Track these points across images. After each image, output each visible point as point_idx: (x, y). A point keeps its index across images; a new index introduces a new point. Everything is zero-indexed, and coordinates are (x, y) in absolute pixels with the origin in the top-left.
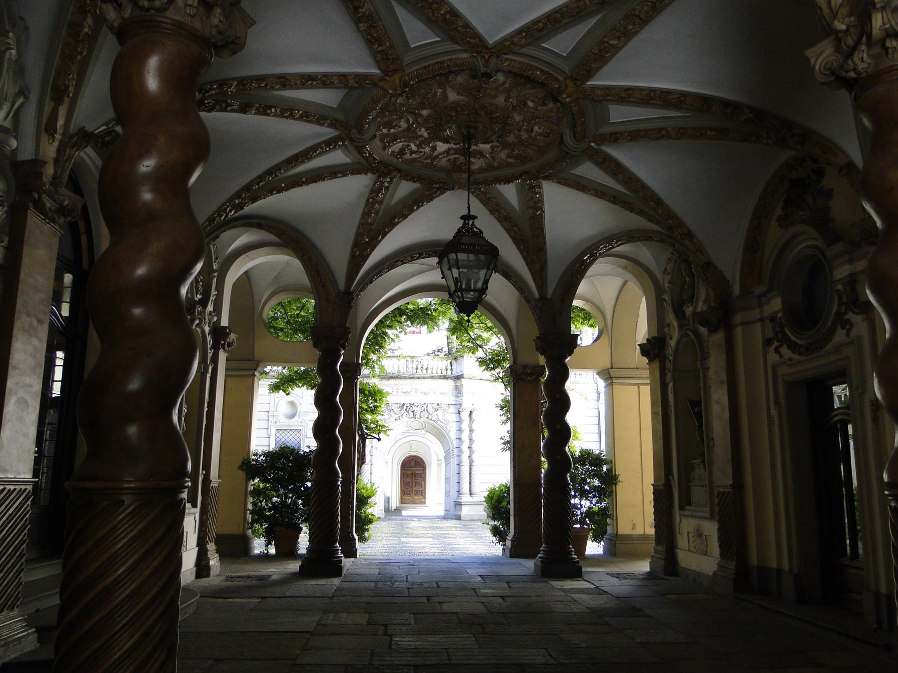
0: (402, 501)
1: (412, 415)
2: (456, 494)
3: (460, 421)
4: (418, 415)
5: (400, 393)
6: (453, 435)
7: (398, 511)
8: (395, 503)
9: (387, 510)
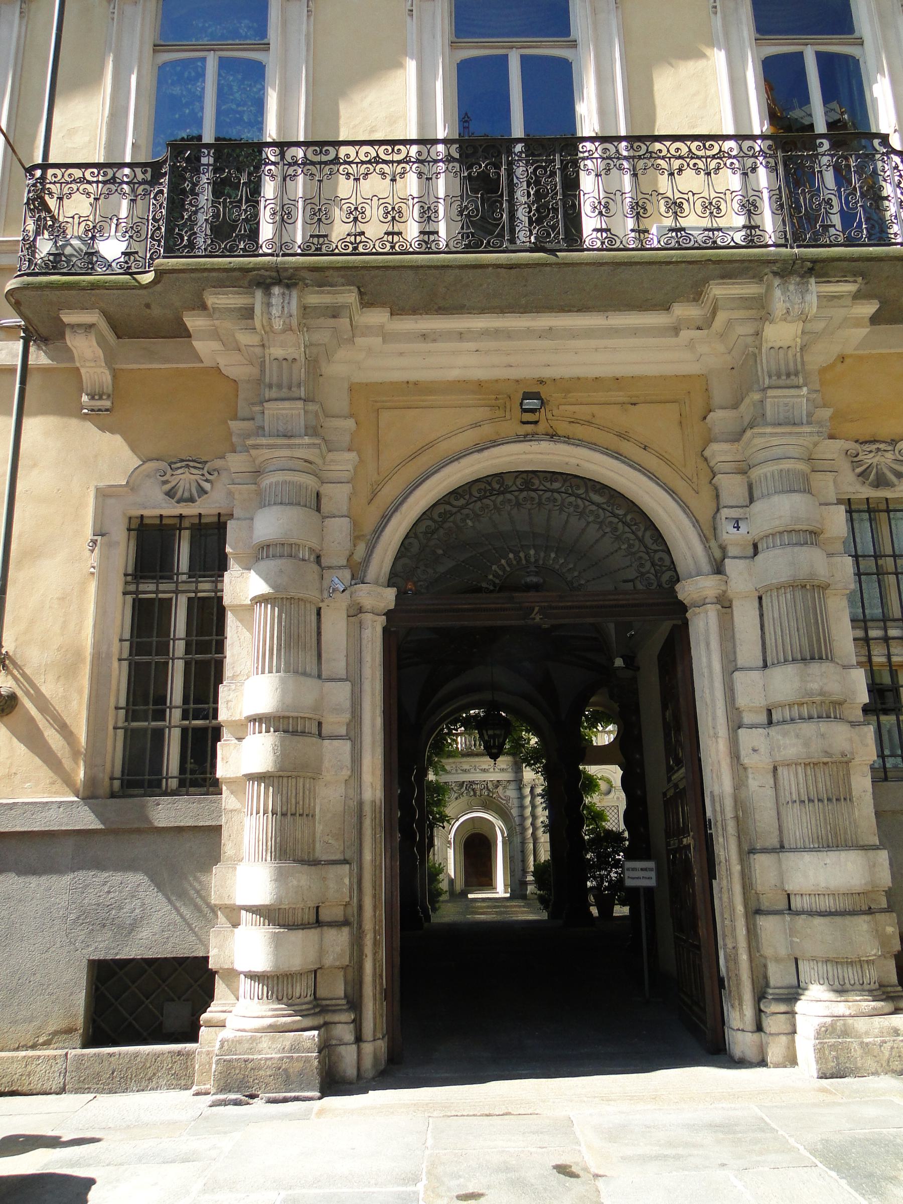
0: (467, 883)
1: (472, 793)
2: (520, 873)
3: (522, 797)
4: (478, 793)
5: (459, 771)
6: (515, 812)
7: (464, 894)
8: (459, 886)
9: (452, 892)
